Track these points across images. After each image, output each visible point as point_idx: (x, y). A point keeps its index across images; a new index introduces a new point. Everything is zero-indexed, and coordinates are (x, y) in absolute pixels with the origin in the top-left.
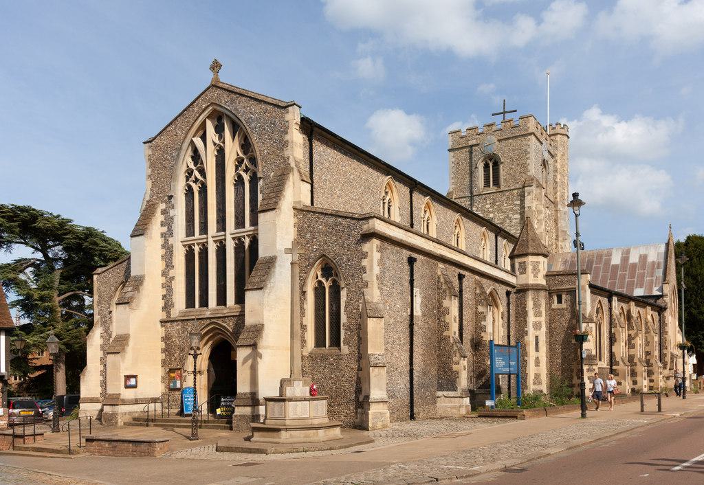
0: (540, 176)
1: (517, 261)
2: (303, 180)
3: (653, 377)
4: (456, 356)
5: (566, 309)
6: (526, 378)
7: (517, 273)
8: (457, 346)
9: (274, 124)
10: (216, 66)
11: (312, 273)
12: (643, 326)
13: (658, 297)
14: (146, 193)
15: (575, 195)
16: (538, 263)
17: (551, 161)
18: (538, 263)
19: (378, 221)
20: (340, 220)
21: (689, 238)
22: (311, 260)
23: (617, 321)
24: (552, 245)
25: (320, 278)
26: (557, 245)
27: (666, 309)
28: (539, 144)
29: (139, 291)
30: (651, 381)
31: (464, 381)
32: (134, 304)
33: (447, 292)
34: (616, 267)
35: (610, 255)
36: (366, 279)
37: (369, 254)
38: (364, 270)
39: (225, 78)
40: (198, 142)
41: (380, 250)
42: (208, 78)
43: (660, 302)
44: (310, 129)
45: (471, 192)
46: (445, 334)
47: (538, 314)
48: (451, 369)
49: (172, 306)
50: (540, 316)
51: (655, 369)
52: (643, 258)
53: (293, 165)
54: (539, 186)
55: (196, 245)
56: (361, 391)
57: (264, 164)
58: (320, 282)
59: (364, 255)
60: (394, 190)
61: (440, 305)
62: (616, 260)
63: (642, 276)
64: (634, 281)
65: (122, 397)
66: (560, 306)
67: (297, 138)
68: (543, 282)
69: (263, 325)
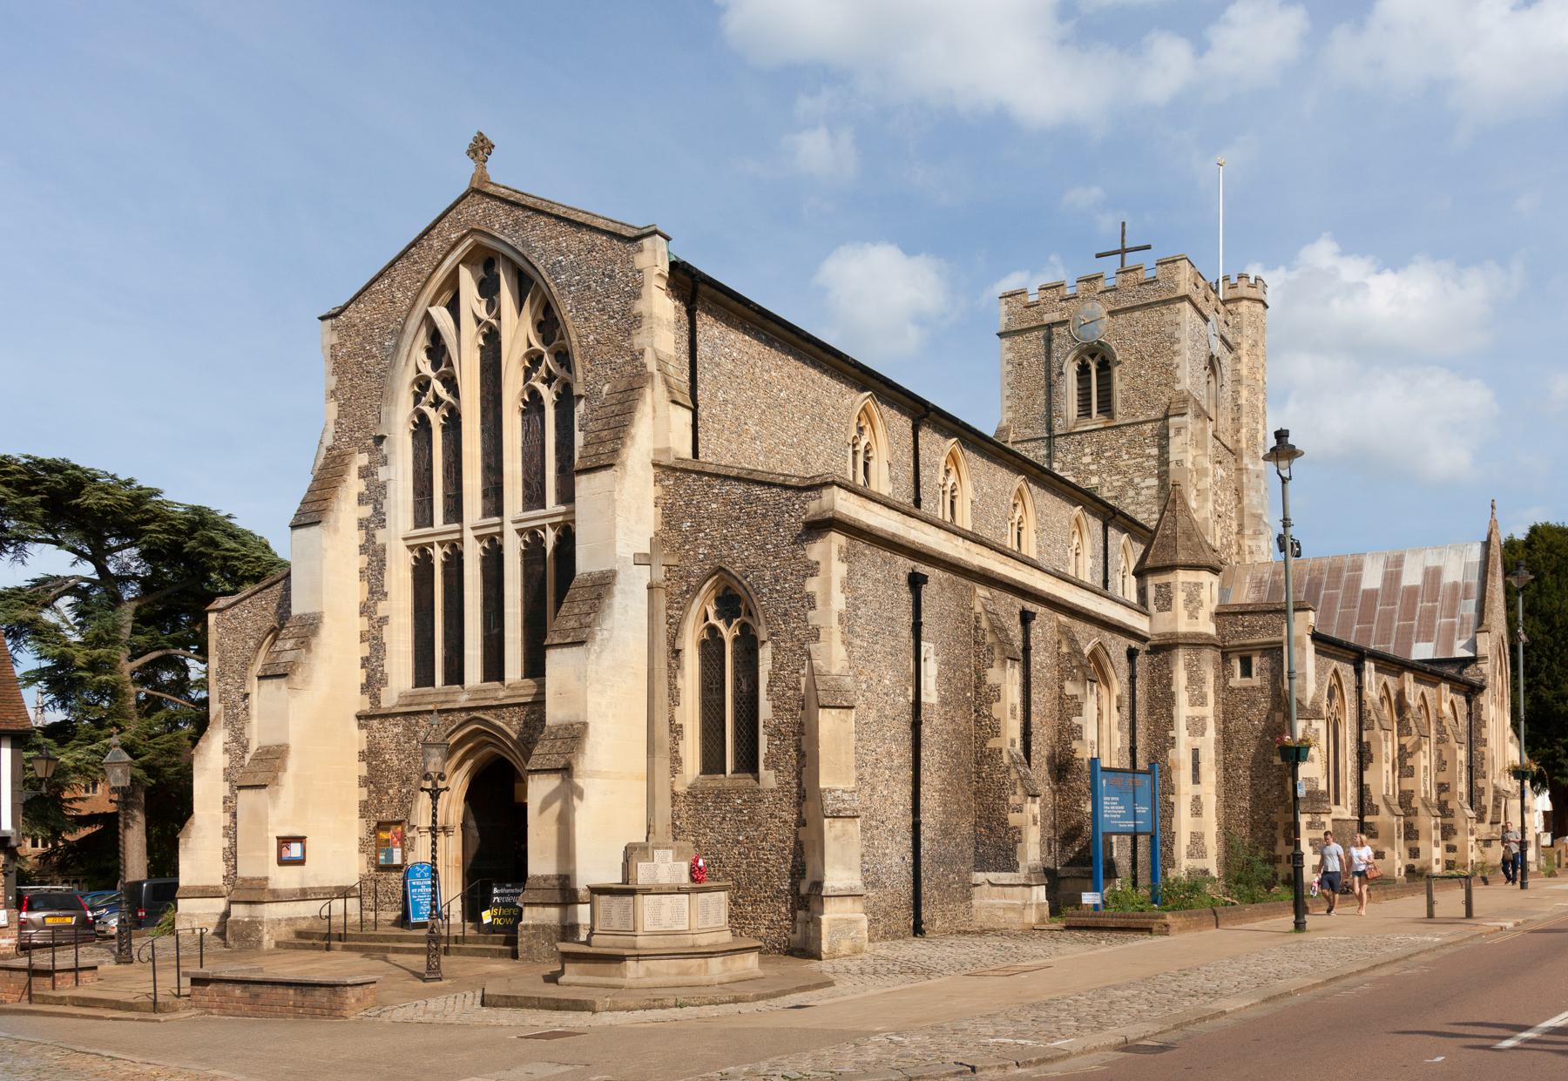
1: (1152, 582)
3: (1455, 841)
4: (1015, 793)
5: (1262, 689)
7: (1152, 607)
8: (1018, 772)
9: (610, 277)
10: (481, 148)
15: (1281, 435)
16: (1199, 585)
17: (1227, 359)
18: (1199, 585)
20: (757, 490)
21: (1534, 530)
23: (1373, 717)
24: (1229, 546)
25: (712, 620)
29: (309, 649)
30: (1450, 849)
31: (1032, 850)
32: (297, 678)
33: (997, 651)
34: (1371, 595)
35: (1358, 567)
37: (822, 566)
38: (810, 600)
40: (441, 315)
41: (847, 557)
42: (462, 174)
43: (1470, 673)
45: (1050, 429)
46: (992, 744)
48: (1004, 823)
49: (383, 681)
50: (1203, 703)
52: (1433, 575)
53: (652, 366)
54: (1201, 414)
55: (436, 545)
57: (589, 366)
58: (713, 630)
59: (812, 569)
61: (980, 680)
63: (1431, 614)
65: (271, 885)
66: (1246, 682)
67: (661, 306)
68: (1211, 629)
69: (585, 724)
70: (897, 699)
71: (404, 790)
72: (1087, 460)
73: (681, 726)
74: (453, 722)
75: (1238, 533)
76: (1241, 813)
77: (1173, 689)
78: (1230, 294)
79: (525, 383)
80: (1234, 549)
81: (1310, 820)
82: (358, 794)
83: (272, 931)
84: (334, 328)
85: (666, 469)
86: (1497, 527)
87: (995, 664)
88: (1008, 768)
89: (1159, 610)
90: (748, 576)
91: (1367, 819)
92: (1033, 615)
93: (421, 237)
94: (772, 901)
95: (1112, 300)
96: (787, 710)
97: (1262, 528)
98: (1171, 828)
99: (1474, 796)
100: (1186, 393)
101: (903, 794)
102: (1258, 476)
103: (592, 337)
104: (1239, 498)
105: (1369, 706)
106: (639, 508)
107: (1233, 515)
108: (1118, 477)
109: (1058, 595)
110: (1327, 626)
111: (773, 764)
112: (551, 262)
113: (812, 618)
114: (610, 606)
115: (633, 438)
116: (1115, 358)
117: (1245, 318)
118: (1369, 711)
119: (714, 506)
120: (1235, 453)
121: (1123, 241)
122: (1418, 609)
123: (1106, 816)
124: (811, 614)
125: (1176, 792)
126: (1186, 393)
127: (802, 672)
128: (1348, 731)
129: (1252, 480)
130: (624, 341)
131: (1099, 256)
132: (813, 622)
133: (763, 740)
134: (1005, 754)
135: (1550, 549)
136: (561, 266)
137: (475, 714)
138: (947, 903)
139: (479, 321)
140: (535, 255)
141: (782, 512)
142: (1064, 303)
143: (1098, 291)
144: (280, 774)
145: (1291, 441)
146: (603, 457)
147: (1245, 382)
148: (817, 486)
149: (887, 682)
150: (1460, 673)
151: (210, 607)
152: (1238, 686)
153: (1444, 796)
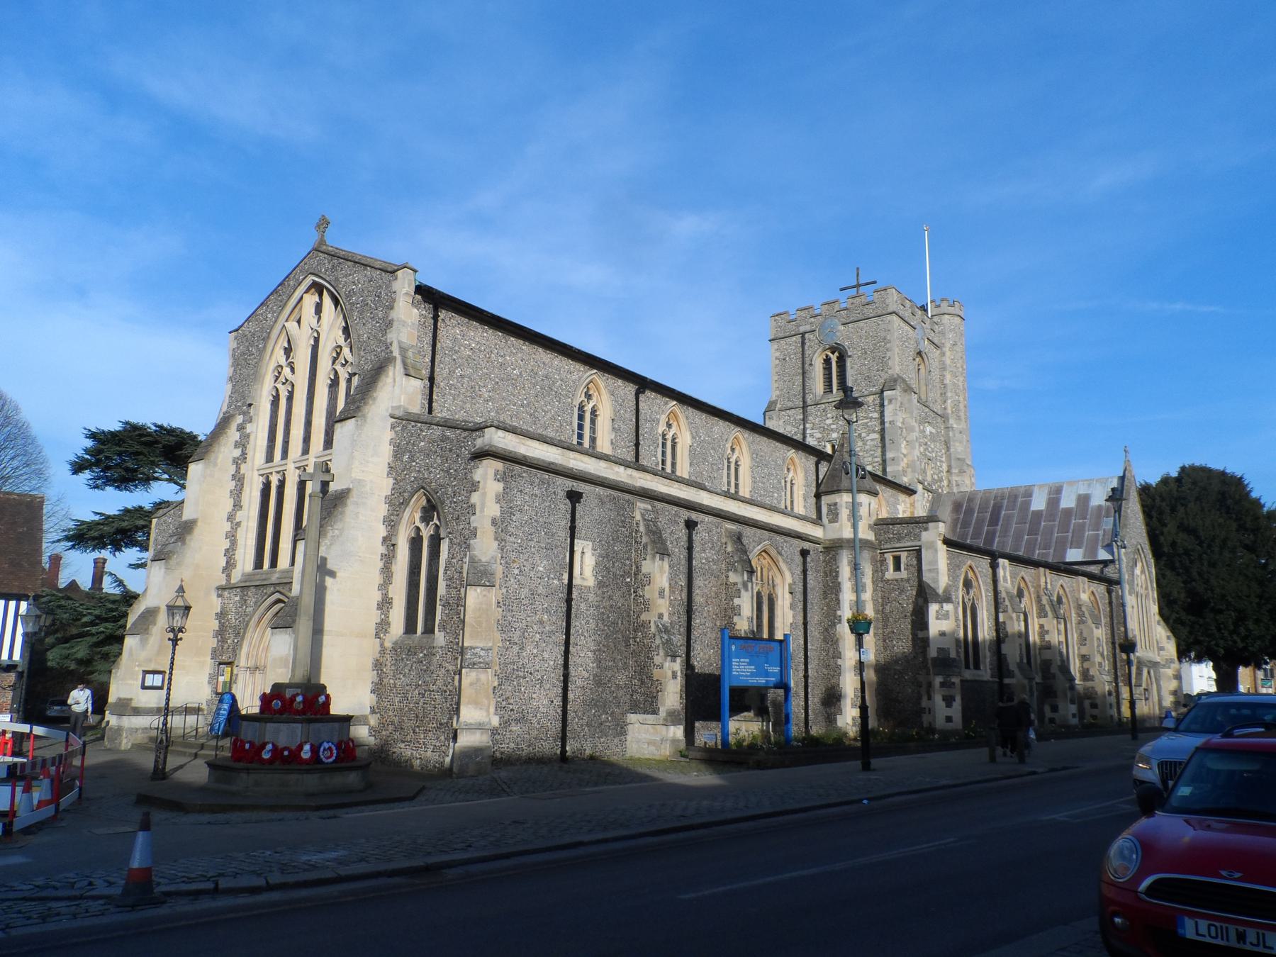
0: (913, 375)
1: (826, 500)
5: (908, 580)
8: (661, 638)
9: (378, 297)
10: (323, 224)
11: (408, 512)
12: (1073, 612)
13: (1105, 563)
14: (224, 401)
17: (934, 354)
21: (1183, 468)
23: (1007, 603)
24: (941, 480)
25: (418, 523)
26: (949, 481)
28: (907, 328)
29: (184, 542)
31: (672, 695)
32: (173, 562)
33: (649, 548)
34: (1038, 514)
35: (1028, 494)
36: (474, 525)
37: (481, 485)
39: (337, 240)
41: (502, 477)
42: (312, 239)
43: (1110, 572)
44: (431, 298)
45: (804, 402)
46: (644, 617)
48: (650, 678)
49: (234, 566)
52: (1084, 500)
53: (396, 353)
54: (908, 389)
57: (362, 353)
58: (418, 529)
59: (474, 486)
62: (1039, 503)
63: (1081, 528)
64: (1036, 540)
65: (134, 704)
68: (870, 536)
70: (551, 581)
71: (236, 641)
72: (829, 421)
73: (840, 666)
75: (948, 471)
76: (895, 674)
77: (840, 580)
78: (937, 311)
79: (286, 361)
80: (945, 483)
81: (942, 680)
82: (213, 643)
83: (129, 737)
85: (403, 420)
86: (1130, 465)
87: (648, 558)
88: (654, 635)
89: (830, 522)
90: (438, 492)
91: (1007, 681)
92: (696, 524)
93: (284, 280)
94: (436, 731)
95: (845, 316)
96: (454, 588)
97: (965, 468)
101: (553, 655)
102: (961, 433)
103: (366, 336)
104: (947, 447)
105: (1003, 595)
106: (375, 445)
107: (943, 459)
109: (725, 509)
110: (1004, 536)
111: (443, 628)
112: (348, 290)
114: (343, 513)
115: (374, 399)
116: (847, 354)
118: (1004, 599)
120: (944, 417)
121: (858, 280)
122: (1072, 526)
123: (734, 673)
124: (473, 518)
125: (842, 657)
127: (464, 560)
128: (985, 612)
129: (957, 435)
130: (382, 337)
131: (842, 290)
132: (473, 525)
133: (439, 609)
135: (1194, 483)
136: (354, 292)
138: (598, 737)
140: (341, 286)
141: (461, 447)
143: (835, 311)
144: (150, 627)
146: (351, 412)
147: (948, 368)
148: (479, 428)
149: (541, 569)
151: (153, 516)
152: (892, 578)
153: (1086, 665)
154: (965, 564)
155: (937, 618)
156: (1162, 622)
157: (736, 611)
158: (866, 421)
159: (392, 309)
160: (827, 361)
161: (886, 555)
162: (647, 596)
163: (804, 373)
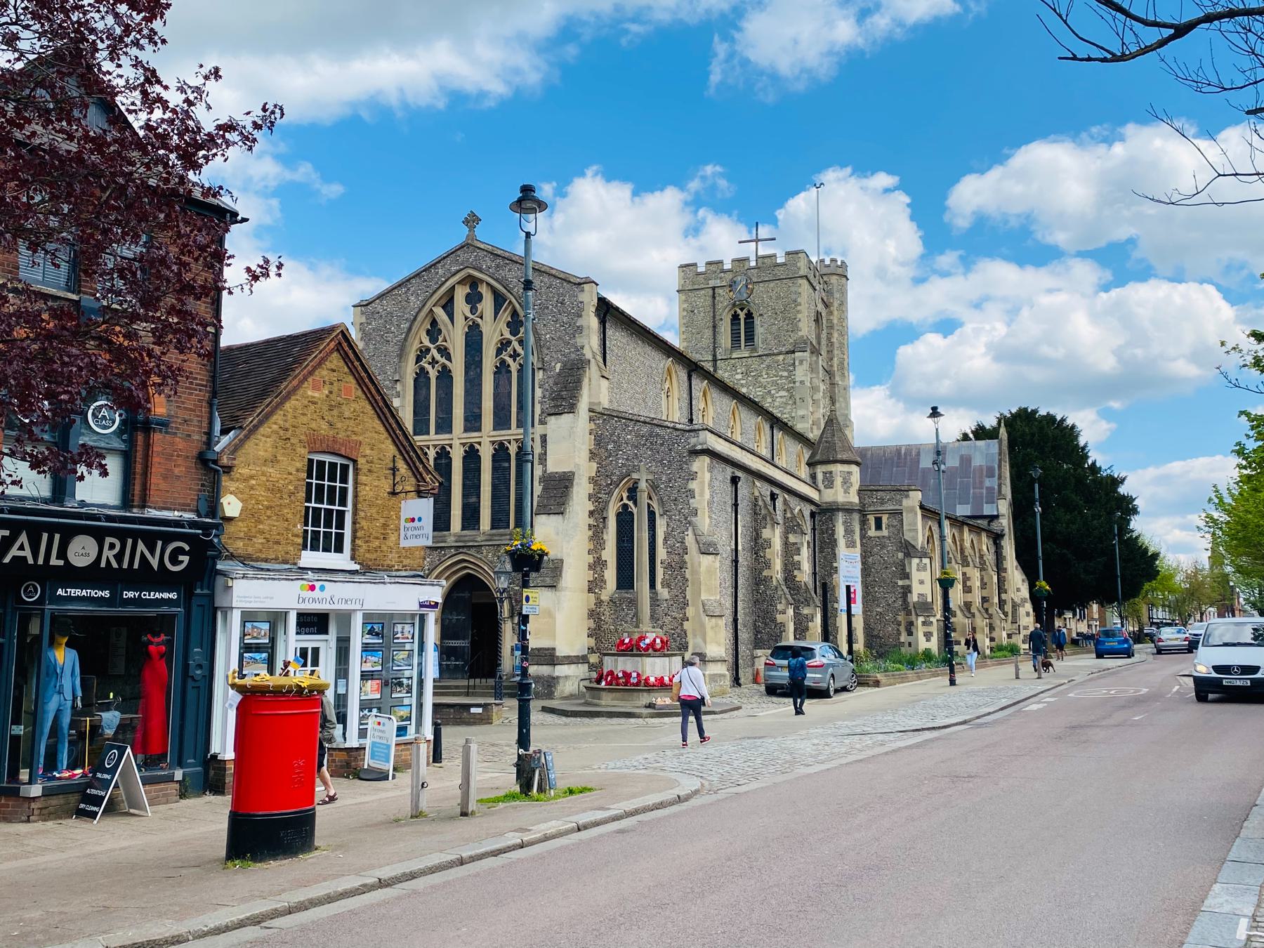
1: (820, 470)
2: (603, 377)
3: (994, 635)
4: (780, 603)
5: (889, 538)
6: (837, 633)
10: (472, 221)
16: (850, 473)
18: (850, 473)
19: (709, 435)
20: (658, 430)
22: (615, 478)
27: (1004, 535)
30: (992, 639)
38: (691, 494)
39: (484, 235)
40: (440, 313)
41: (711, 470)
43: (995, 526)
44: (606, 310)
45: (714, 356)
46: (765, 573)
47: (851, 544)
48: (774, 620)
51: (997, 622)
55: (431, 447)
56: (687, 647)
58: (625, 506)
59: (693, 476)
60: (674, 376)
66: (879, 533)
68: (856, 500)
69: (562, 561)
72: (739, 377)
73: (606, 561)
74: (445, 555)
84: (362, 313)
87: (768, 526)
88: (777, 588)
98: (835, 624)
99: (1002, 603)
100: (805, 338)
103: (548, 336)
108: (760, 389)
113: (693, 503)
117: (835, 288)
119: (629, 437)
126: (805, 338)
134: (774, 579)
137: (461, 550)
139: (466, 318)
142: (722, 274)
145: (938, 410)
147: (836, 328)
150: (989, 525)
153: (986, 605)
154: (710, 503)
155: (918, 570)
156: (1019, 567)
157: (797, 566)
158: (775, 378)
159: (581, 316)
160: (735, 318)
161: (868, 516)
162: (768, 556)
163: (714, 327)
